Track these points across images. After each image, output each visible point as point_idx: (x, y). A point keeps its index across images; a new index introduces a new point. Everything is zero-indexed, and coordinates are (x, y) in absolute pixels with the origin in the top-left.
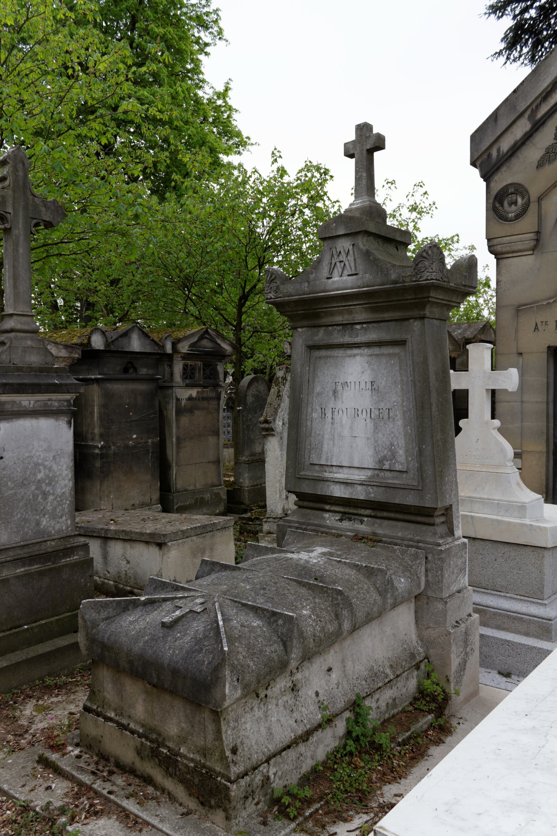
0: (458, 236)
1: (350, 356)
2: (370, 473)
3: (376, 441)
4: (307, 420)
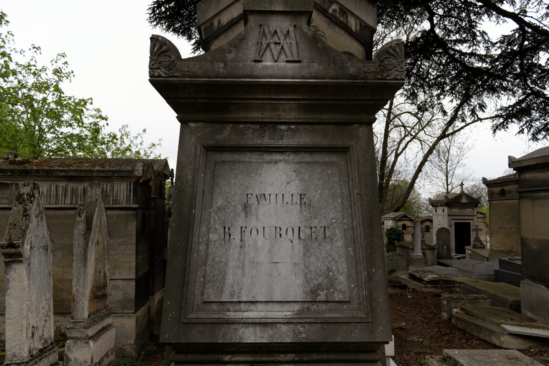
0: (92, 99)
1: (269, 162)
2: (297, 307)
3: (307, 267)
4: (199, 243)
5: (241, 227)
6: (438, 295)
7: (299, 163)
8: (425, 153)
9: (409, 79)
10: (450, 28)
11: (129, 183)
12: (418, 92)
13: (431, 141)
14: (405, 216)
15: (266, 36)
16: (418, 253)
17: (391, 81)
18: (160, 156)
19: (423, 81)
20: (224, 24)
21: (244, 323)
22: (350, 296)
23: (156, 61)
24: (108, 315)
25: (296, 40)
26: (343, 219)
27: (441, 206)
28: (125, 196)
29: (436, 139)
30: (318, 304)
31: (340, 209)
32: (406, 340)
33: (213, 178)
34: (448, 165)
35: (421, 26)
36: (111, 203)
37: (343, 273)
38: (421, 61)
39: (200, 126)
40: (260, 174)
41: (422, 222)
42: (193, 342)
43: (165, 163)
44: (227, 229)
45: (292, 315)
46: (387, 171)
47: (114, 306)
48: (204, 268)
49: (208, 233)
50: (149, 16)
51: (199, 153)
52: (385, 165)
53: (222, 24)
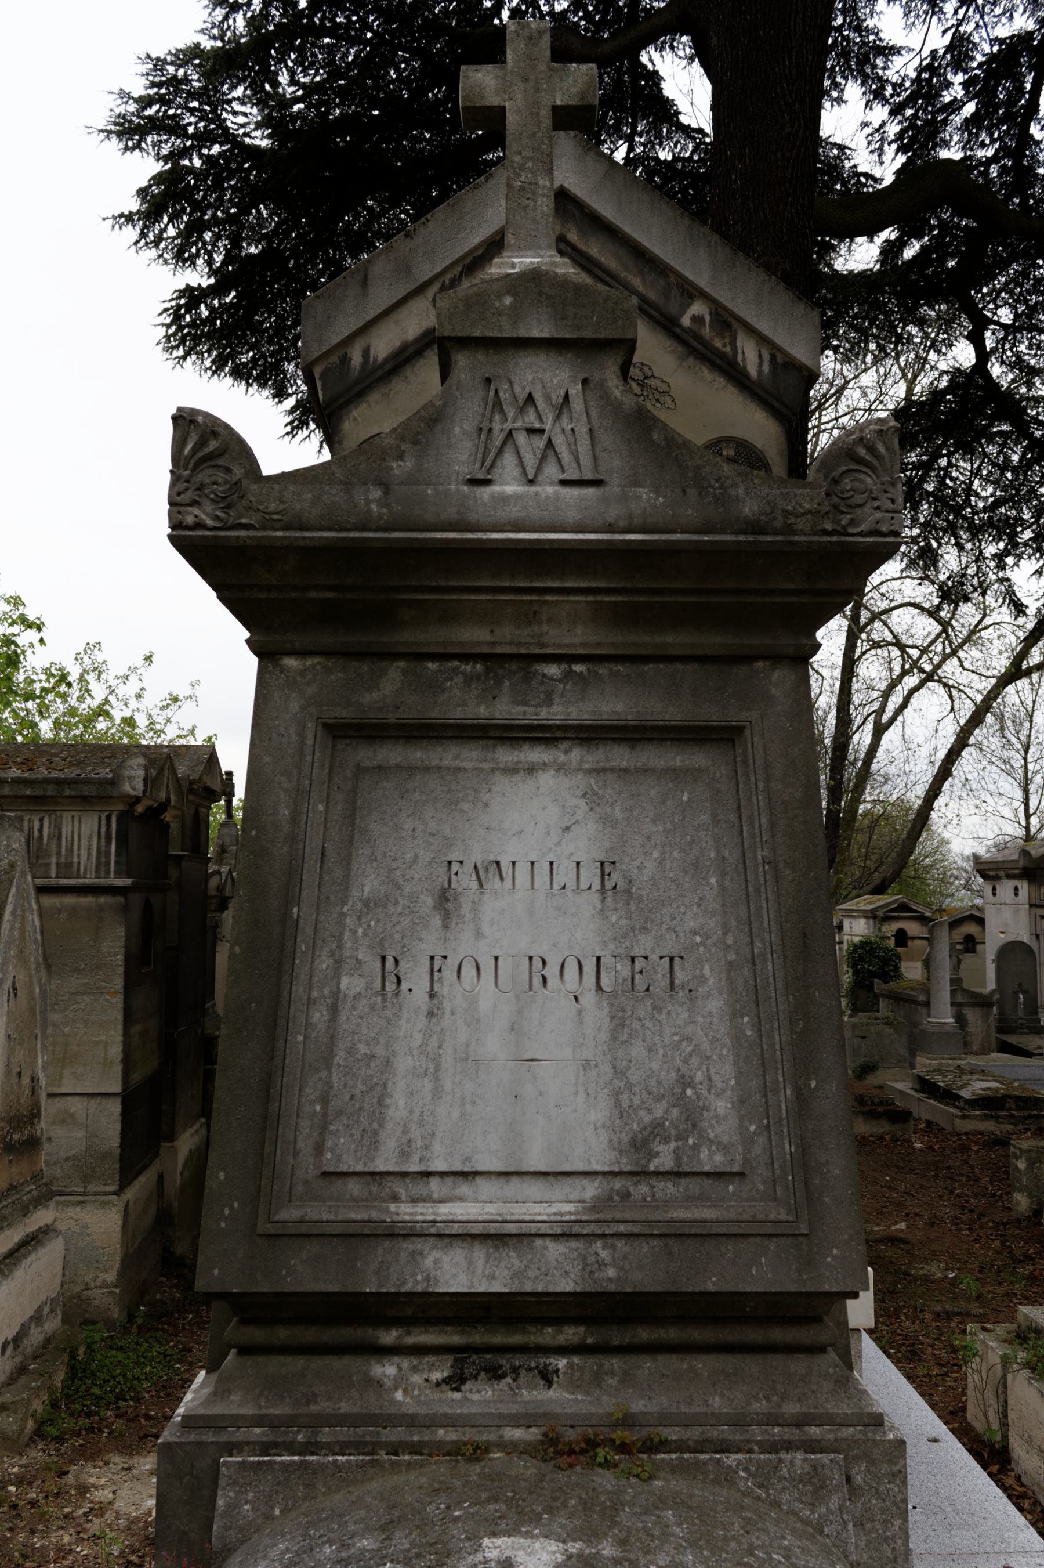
1: (511, 771)
2: (591, 1190)
3: (619, 1073)
4: (310, 1002)
5: (432, 958)
6: (1002, 1142)
7: (598, 771)
8: (962, 722)
9: (915, 508)
10: (1033, 362)
11: (104, 816)
12: (940, 545)
13: (980, 687)
14: (903, 907)
15: (502, 411)
16: (943, 1015)
17: (861, 539)
18: (192, 732)
19: (953, 515)
20: (380, 359)
21: (440, 1236)
22: (745, 1158)
23: (187, 481)
24: (41, 1200)
25: (589, 422)
26: (725, 934)
27: (1009, 877)
28: (94, 853)
29: (993, 681)
30: (653, 1181)
31: (716, 906)
32: (906, 1274)
33: (352, 814)
34: (1029, 760)
35: (949, 356)
36: (53, 874)
37: (723, 1091)
38: (949, 455)
39: (314, 666)
40: (486, 805)
41: (954, 924)
42: (293, 1289)
43: (209, 756)
44: (390, 962)
45: (577, 1213)
46: (850, 774)
47: (58, 1172)
48: (324, 1074)
49: (337, 976)
50: (162, 331)
51: (310, 742)
52: (845, 757)
53: (375, 360)
